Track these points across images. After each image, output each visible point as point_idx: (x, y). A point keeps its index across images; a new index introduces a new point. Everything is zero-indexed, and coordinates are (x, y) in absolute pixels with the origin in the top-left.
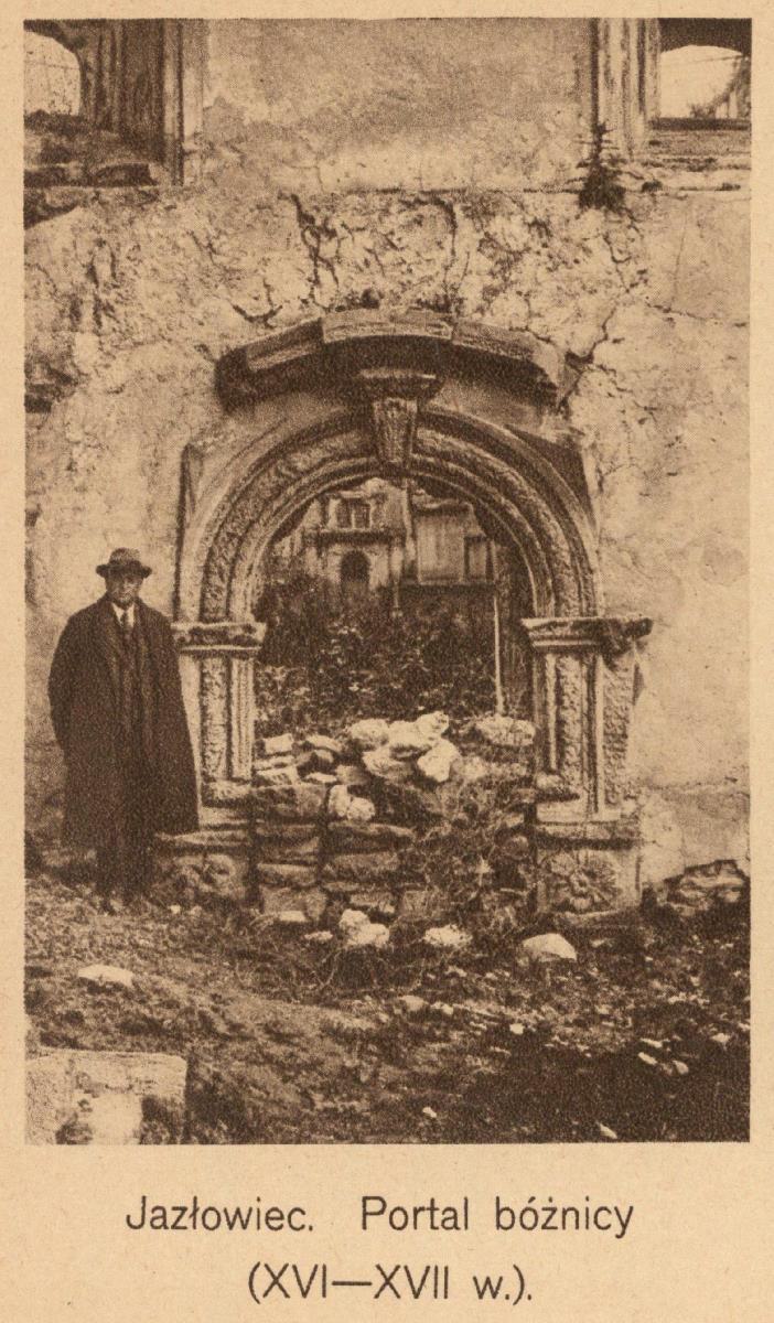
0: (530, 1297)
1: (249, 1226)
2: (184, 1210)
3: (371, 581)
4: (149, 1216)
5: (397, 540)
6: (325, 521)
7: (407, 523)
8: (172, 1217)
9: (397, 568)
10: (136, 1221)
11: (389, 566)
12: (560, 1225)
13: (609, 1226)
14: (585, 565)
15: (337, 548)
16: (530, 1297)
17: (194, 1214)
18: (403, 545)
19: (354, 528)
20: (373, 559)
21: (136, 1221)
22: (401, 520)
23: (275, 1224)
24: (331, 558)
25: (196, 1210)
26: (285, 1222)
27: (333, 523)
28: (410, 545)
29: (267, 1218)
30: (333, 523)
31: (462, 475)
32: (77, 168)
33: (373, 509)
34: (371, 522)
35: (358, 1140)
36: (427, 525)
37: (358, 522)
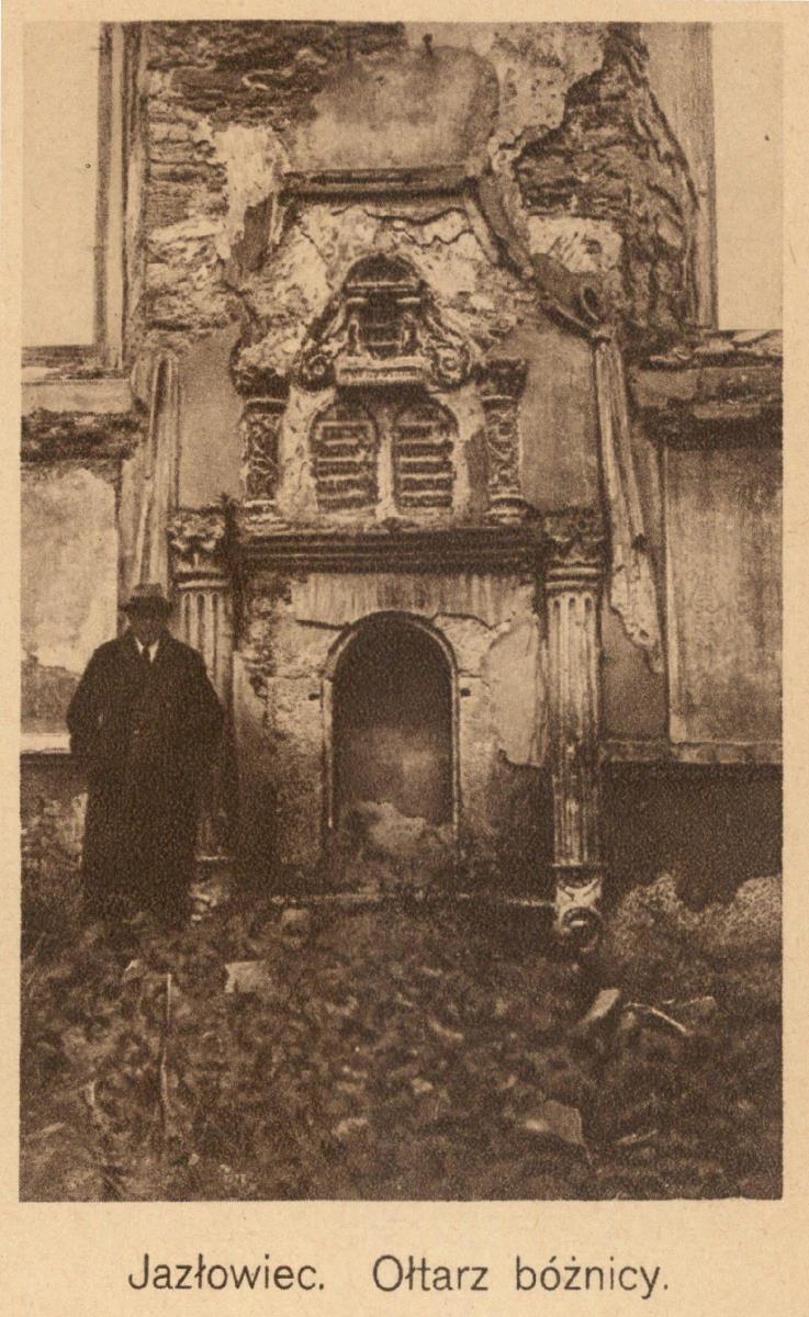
0: (666, 1287)
1: (257, 1283)
2: (188, 1268)
4: (152, 1275)
8: (176, 1275)
10: (138, 1281)
12: (583, 1285)
13: (635, 1286)
16: (666, 1287)
17: (199, 1275)
21: (138, 1281)
23: (284, 1282)
25: (202, 1268)
26: (295, 1281)
29: (277, 1277)
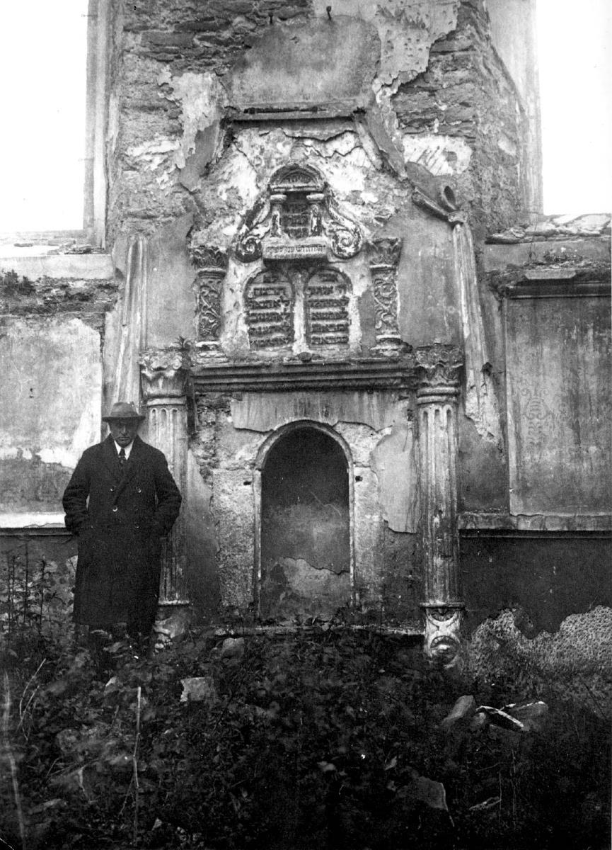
3: (356, 510)
5: (440, 384)
6: (213, 329)
7: (471, 328)
9: (439, 472)
11: (416, 463)
14: (461, 411)
15: (245, 412)
18: (458, 398)
19: (300, 346)
20: (359, 444)
22: (454, 323)
24: (231, 439)
27: (236, 331)
28: (481, 402)
30: (236, 331)
31: (331, 314)
32: (383, 684)
33: (360, 286)
34: (355, 333)
35: (88, 93)
36: (535, 340)
37: (312, 333)
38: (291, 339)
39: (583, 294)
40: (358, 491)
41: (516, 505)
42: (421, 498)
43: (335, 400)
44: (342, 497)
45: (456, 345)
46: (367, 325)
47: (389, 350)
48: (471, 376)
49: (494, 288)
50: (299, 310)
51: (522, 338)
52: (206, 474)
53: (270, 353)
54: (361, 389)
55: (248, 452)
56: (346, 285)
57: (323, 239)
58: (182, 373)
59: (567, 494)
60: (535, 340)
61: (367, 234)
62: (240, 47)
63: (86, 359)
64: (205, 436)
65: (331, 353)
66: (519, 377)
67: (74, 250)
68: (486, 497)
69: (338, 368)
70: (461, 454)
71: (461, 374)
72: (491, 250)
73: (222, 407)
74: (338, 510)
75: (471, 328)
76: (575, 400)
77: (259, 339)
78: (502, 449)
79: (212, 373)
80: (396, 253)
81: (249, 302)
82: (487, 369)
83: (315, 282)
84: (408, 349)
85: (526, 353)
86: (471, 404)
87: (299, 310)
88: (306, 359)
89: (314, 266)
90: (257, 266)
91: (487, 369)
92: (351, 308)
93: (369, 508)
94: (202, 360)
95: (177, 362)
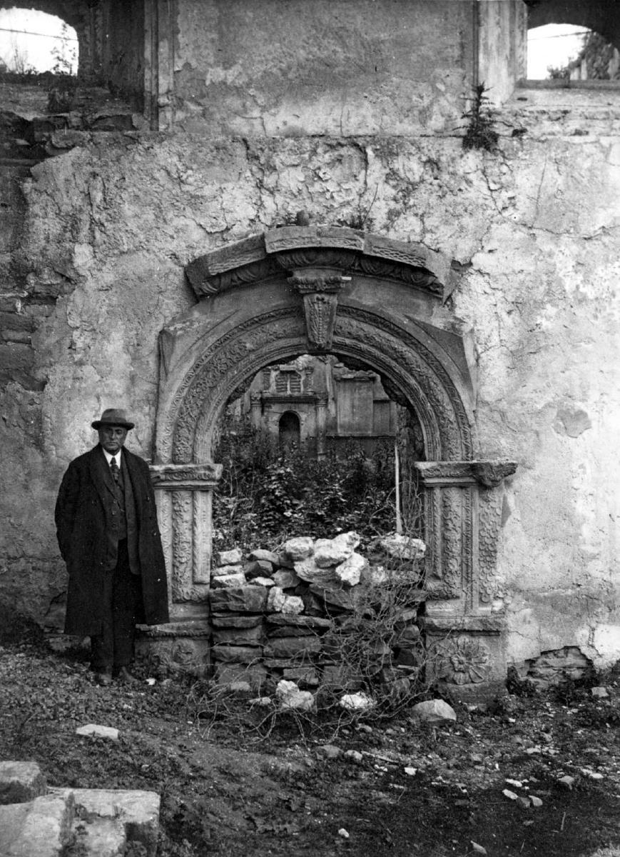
3: (302, 432)
5: (322, 402)
7: (329, 388)
9: (321, 423)
18: (326, 406)
19: (289, 392)
20: (303, 416)
22: (326, 387)
27: (273, 388)
28: (332, 407)
33: (303, 378)
34: (302, 389)
36: (345, 391)
38: (286, 390)
39: (355, 381)
40: (302, 428)
41: (339, 430)
42: (317, 430)
43: (297, 405)
44: (298, 429)
45: (326, 393)
46: (305, 387)
47: (310, 394)
48: (329, 400)
49: (335, 379)
50: (288, 383)
51: (342, 392)
52: (266, 423)
53: (282, 394)
54: (304, 403)
55: (276, 418)
56: (300, 377)
57: (295, 366)
58: (261, 399)
59: (350, 427)
60: (345, 391)
61: (306, 365)
62: (202, 472)
63: (525, 137)
64: (265, 414)
65: (296, 394)
66: (340, 399)
67: (345, 715)
68: (332, 428)
69: (298, 398)
70: (327, 419)
71: (327, 400)
72: (335, 369)
73: (270, 407)
74: (296, 433)
75: (329, 388)
76: (353, 406)
77: (279, 390)
78: (336, 418)
79: (267, 398)
80: (312, 370)
81: (276, 381)
82: (333, 399)
83: (293, 376)
84: (315, 393)
85: (342, 392)
86: (329, 407)
87: (288, 383)
88: (291, 396)
89: (293, 372)
90: (278, 372)
91: (333, 399)
92: (301, 383)
93: (305, 431)
94: (266, 395)
95: (260, 396)
